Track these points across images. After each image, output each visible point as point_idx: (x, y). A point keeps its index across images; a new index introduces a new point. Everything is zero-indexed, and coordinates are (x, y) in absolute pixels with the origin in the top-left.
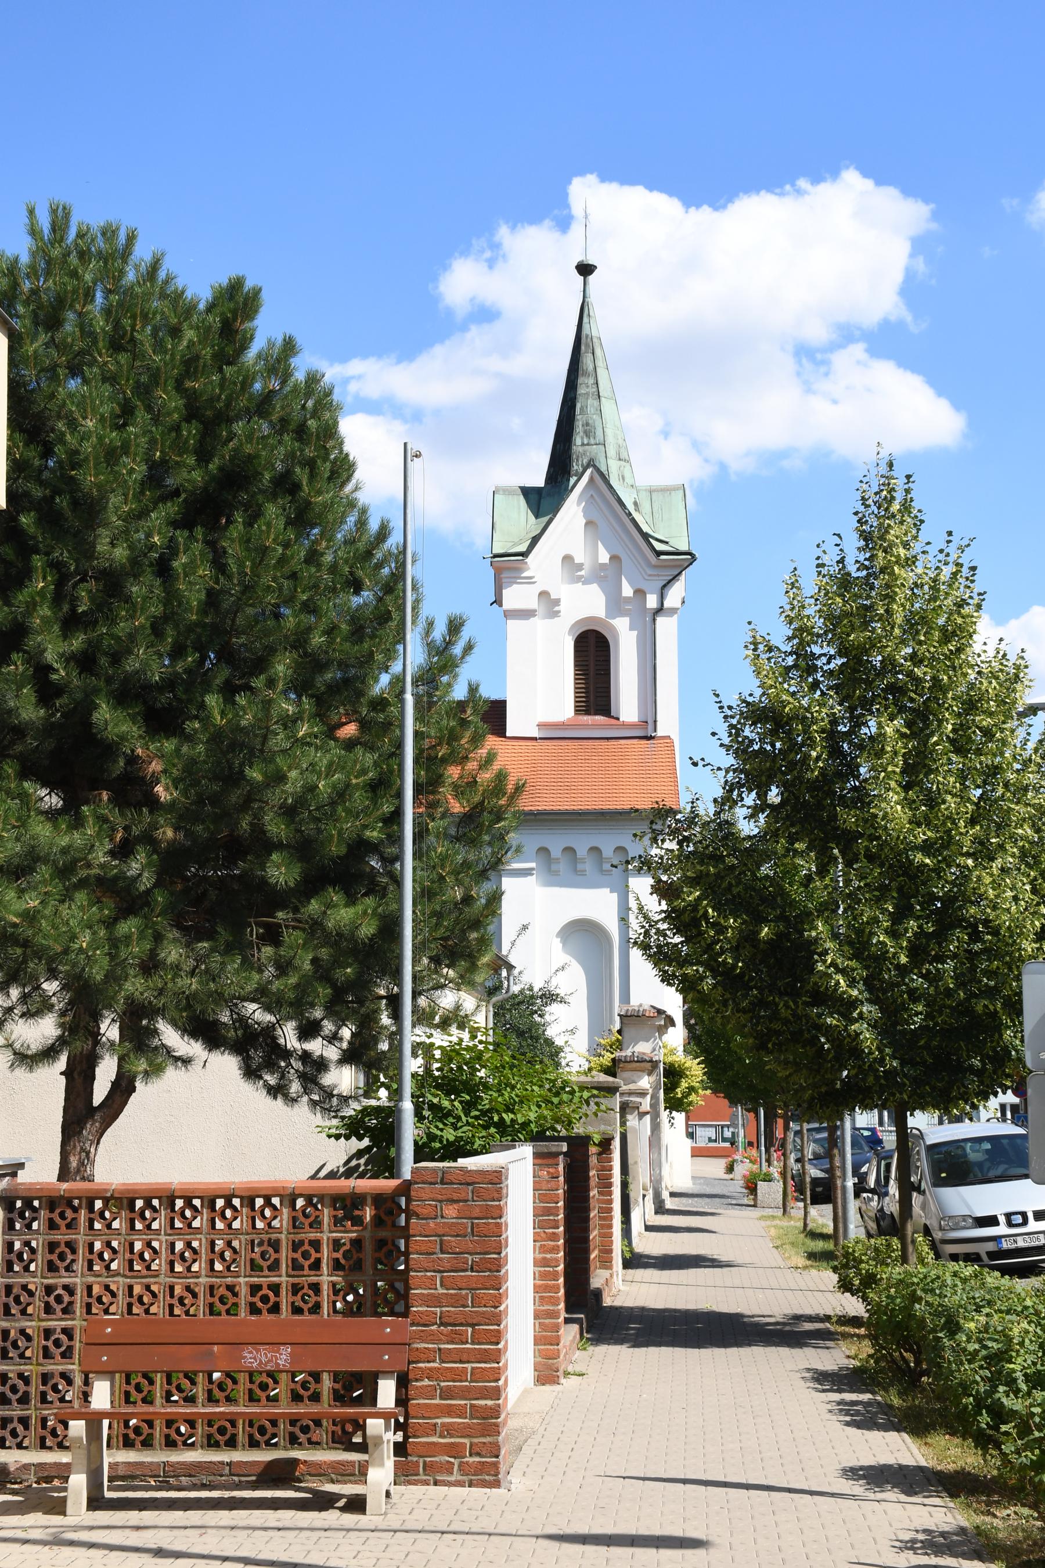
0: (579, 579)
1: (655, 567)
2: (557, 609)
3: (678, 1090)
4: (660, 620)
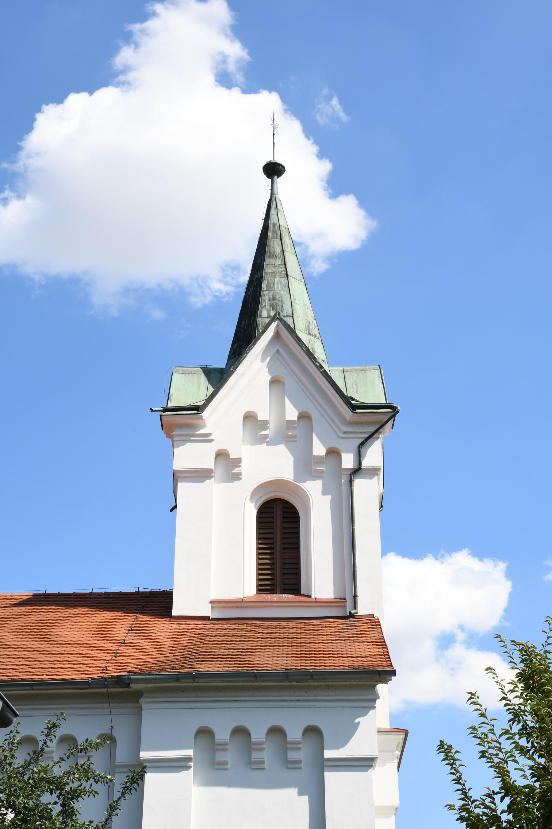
0: (263, 439)
2: (237, 470)
4: (358, 483)
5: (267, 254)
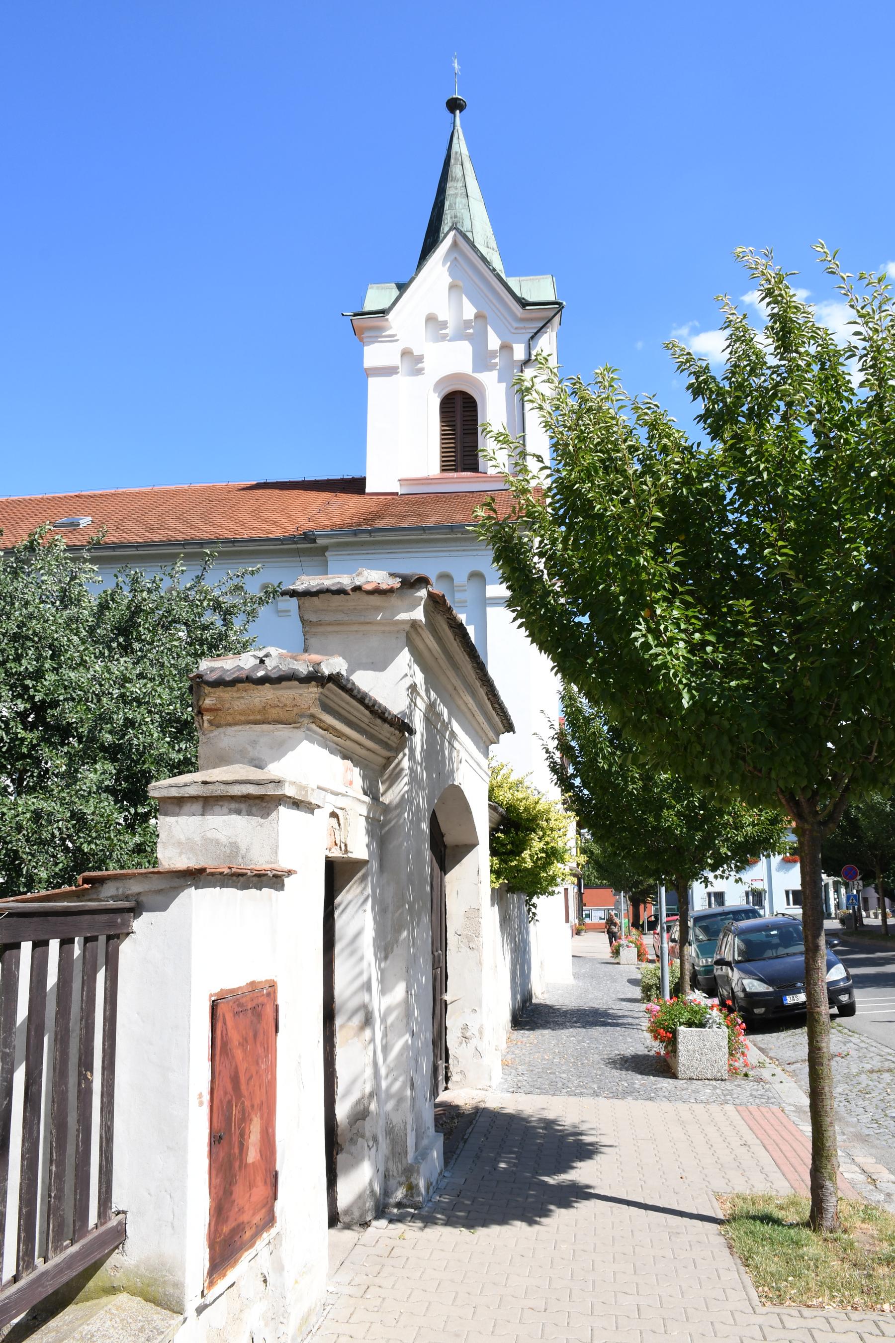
0: (444, 338)
1: (523, 320)
2: (420, 366)
3: (526, 854)
5: (449, 178)
